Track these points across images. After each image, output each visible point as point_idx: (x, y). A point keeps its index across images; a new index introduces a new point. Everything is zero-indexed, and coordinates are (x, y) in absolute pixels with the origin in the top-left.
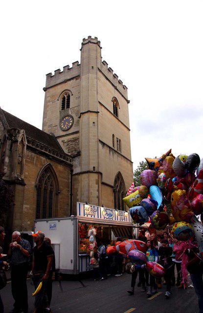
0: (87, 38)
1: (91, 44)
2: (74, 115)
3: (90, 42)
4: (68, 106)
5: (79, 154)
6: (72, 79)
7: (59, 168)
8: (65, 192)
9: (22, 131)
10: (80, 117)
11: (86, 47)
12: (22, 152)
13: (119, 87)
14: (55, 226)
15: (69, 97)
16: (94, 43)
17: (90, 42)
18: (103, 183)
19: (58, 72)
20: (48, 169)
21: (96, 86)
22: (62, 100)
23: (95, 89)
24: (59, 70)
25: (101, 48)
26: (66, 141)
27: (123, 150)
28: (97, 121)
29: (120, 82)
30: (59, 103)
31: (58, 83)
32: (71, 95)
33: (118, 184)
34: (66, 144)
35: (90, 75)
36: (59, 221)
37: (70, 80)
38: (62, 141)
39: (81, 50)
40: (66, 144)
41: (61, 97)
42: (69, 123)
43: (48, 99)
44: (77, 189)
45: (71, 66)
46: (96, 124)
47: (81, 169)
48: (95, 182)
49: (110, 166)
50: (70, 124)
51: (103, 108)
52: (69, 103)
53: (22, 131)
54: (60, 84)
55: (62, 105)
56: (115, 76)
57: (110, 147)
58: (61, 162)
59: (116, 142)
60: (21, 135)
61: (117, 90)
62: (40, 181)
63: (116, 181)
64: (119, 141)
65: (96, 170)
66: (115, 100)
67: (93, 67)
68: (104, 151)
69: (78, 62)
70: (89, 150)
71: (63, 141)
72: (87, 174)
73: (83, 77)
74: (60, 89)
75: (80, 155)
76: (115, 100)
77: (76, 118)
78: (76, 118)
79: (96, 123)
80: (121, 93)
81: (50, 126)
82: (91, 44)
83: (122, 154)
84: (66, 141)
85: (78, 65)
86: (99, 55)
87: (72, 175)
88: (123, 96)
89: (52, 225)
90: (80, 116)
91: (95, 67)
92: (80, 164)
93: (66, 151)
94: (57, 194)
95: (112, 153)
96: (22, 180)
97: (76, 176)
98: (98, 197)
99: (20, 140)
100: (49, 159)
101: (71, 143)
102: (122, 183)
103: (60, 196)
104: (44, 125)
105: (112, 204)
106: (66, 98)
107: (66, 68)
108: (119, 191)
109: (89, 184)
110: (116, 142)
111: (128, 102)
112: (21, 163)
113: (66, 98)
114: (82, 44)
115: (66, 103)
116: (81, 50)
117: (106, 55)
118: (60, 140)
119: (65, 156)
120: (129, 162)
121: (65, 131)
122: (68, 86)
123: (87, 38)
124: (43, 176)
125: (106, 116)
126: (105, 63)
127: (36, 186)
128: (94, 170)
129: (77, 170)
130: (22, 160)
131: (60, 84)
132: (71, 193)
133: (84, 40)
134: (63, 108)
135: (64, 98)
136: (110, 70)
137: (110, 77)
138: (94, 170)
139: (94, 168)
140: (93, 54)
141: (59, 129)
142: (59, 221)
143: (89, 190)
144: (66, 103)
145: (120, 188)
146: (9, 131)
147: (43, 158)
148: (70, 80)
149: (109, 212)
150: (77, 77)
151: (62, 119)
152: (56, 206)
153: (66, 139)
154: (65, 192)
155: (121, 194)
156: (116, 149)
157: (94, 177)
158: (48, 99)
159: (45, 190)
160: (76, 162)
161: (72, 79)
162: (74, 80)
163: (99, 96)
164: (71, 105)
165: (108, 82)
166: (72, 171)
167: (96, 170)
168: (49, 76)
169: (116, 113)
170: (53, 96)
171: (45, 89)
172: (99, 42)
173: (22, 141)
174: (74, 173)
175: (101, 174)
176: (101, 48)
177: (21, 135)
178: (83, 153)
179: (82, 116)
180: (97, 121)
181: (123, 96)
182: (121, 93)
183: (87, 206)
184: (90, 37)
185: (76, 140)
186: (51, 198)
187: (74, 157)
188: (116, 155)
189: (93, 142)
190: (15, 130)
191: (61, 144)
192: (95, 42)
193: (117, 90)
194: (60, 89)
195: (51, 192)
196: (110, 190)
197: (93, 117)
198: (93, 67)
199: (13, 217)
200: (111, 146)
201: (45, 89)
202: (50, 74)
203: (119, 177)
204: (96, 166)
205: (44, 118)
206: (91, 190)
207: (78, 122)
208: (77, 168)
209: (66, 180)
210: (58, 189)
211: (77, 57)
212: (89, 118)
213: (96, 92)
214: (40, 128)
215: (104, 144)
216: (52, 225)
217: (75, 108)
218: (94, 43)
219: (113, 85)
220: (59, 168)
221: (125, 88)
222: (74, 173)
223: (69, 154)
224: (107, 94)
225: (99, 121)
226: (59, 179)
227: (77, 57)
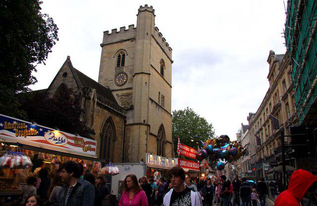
0: (143, 6)
1: (146, 12)
2: (128, 73)
3: (146, 10)
4: (123, 64)
5: (132, 108)
6: (128, 40)
7: (116, 119)
8: (120, 139)
9: (94, 90)
10: (134, 76)
11: (142, 14)
12: (93, 107)
13: (166, 50)
14: (129, 169)
15: (124, 56)
16: (150, 12)
17: (146, 10)
18: (151, 134)
19: (114, 30)
20: (109, 120)
21: (149, 50)
22: (117, 58)
23: (149, 54)
24: (116, 29)
25: (155, 16)
26: (120, 94)
27: (165, 105)
28: (149, 82)
29: (167, 45)
30: (115, 60)
31: (114, 41)
32: (126, 55)
33: (161, 134)
34: (120, 98)
35: (145, 41)
36: (132, 165)
37: (126, 41)
38: (117, 95)
39: (137, 15)
40: (120, 98)
41: (117, 55)
42: (124, 79)
43: (104, 55)
44: (129, 137)
45: (127, 28)
46: (148, 84)
47: (133, 121)
48: (144, 133)
49: (156, 119)
50: (125, 81)
51: (154, 70)
52: (124, 62)
53: (94, 90)
54: (117, 42)
55: (118, 63)
56: (164, 40)
57: (157, 104)
58: (118, 114)
59: (161, 99)
60: (93, 93)
61: (164, 52)
62: (103, 131)
63: (159, 132)
64: (163, 97)
65: (146, 122)
66: (162, 61)
67: (147, 33)
68: (152, 106)
69: (133, 25)
70: (141, 105)
71: (117, 95)
72: (138, 126)
73: (139, 41)
74: (117, 47)
75: (133, 109)
76: (162, 61)
77: (130, 76)
78: (130, 76)
79: (148, 83)
80: (166, 54)
81: (106, 79)
82: (146, 12)
83: (165, 108)
84: (120, 94)
85: (134, 28)
86: (153, 22)
87: (125, 125)
88: (168, 57)
89: (127, 168)
90: (135, 75)
91: (149, 34)
92: (133, 117)
93: (120, 104)
94: (114, 141)
95: (157, 108)
96: (93, 130)
97: (129, 127)
98: (146, 145)
99: (92, 98)
100: (110, 112)
101: (124, 97)
102: (164, 133)
103: (116, 143)
104: (100, 77)
105: (155, 151)
106: (121, 57)
107: (123, 29)
108: (161, 140)
109: (139, 133)
110: (161, 99)
111: (172, 62)
112: (92, 116)
113: (121, 57)
114: (139, 10)
115: (121, 61)
116: (137, 15)
117: (158, 23)
118: (114, 94)
119: (120, 109)
120: (169, 115)
121: (120, 86)
122: (124, 46)
123: (143, 6)
124: (105, 125)
125: (155, 76)
126: (156, 29)
127: (100, 135)
128: (144, 122)
129: (129, 121)
130: (93, 113)
131: (117, 42)
132: (124, 140)
133: (141, 7)
134: (118, 65)
135: (119, 56)
136: (160, 35)
137: (160, 41)
138: (144, 122)
139: (144, 120)
140: (148, 21)
141: (114, 83)
142: (132, 165)
143: (139, 139)
144: (121, 61)
145: (162, 137)
146: (83, 90)
147: (106, 111)
148: (126, 41)
149: (163, 160)
150: (133, 39)
151: (116, 76)
152: (113, 150)
153: (120, 93)
154: (120, 139)
155: (162, 142)
156: (160, 105)
157: (144, 128)
158: (104, 55)
159: (106, 137)
160: (129, 114)
161: (128, 40)
162: (130, 41)
163: (151, 60)
164: (126, 64)
165: (158, 45)
166: (125, 122)
167: (146, 122)
168: (106, 33)
169: (162, 74)
170: (109, 53)
171: (102, 45)
172: (154, 10)
173: (93, 98)
174: (127, 123)
175: (149, 126)
176: (155, 16)
177: (93, 93)
178: (136, 108)
179: (136, 76)
180: (149, 82)
181: (168, 57)
182: (166, 54)
183: (151, 156)
184: (146, 5)
185: (128, 95)
186: (109, 144)
187: (128, 110)
188: (160, 110)
189: (145, 99)
190: (88, 88)
191: (116, 97)
192: (151, 10)
193: (164, 52)
194: (117, 47)
195: (110, 139)
196: (154, 139)
197: (145, 77)
198: (147, 33)
199: (174, 168)
200: (157, 102)
201: (102, 45)
202: (108, 32)
203: (162, 128)
204: (146, 119)
205: (100, 72)
206: (141, 139)
207: (132, 80)
208: (130, 120)
209: (121, 130)
210: (115, 136)
211: (134, 21)
212: (142, 79)
213: (149, 57)
214: (97, 80)
215: (152, 101)
216: (127, 168)
217: (129, 67)
218: (150, 12)
219: (162, 48)
220: (116, 119)
221: (170, 49)
222: (127, 123)
223: (123, 107)
224: (157, 55)
225: (150, 81)
226: (116, 128)
227: (134, 21)
